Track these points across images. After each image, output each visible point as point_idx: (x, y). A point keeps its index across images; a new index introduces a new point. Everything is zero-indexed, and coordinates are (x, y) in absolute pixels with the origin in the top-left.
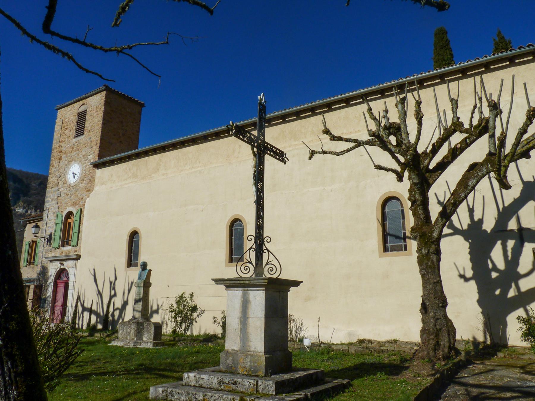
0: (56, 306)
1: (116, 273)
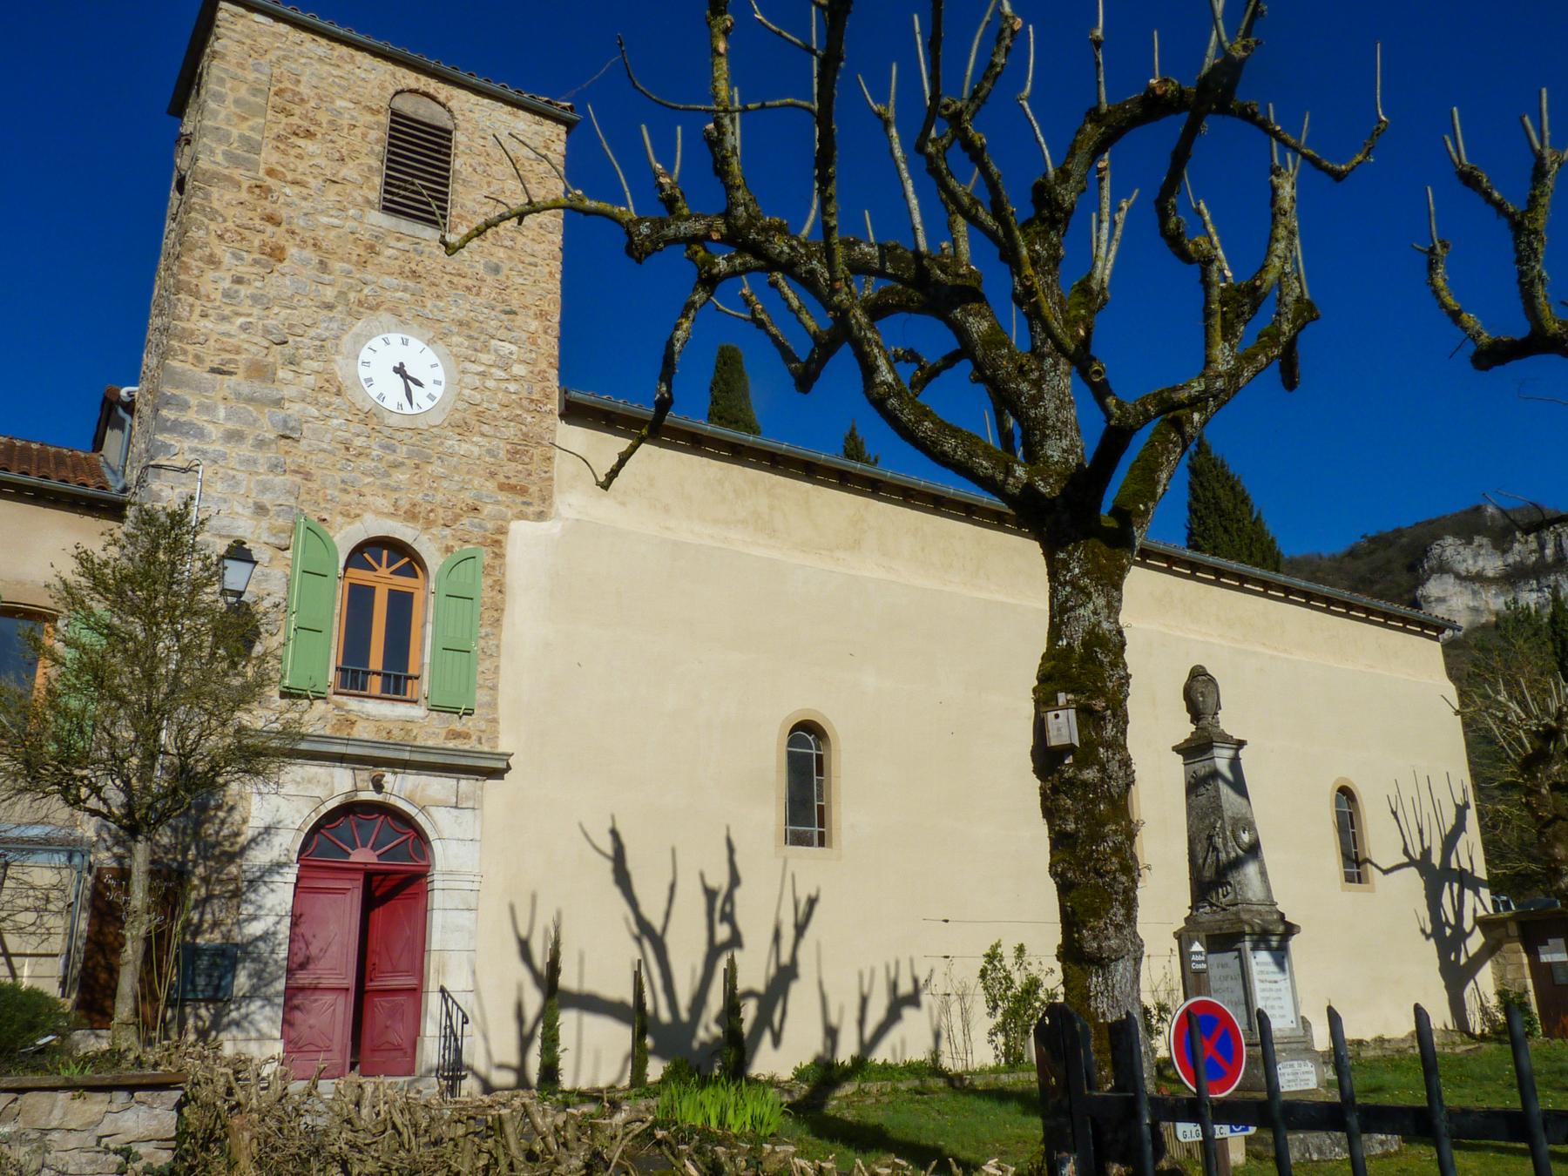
0: (302, 989)
1: (738, 858)
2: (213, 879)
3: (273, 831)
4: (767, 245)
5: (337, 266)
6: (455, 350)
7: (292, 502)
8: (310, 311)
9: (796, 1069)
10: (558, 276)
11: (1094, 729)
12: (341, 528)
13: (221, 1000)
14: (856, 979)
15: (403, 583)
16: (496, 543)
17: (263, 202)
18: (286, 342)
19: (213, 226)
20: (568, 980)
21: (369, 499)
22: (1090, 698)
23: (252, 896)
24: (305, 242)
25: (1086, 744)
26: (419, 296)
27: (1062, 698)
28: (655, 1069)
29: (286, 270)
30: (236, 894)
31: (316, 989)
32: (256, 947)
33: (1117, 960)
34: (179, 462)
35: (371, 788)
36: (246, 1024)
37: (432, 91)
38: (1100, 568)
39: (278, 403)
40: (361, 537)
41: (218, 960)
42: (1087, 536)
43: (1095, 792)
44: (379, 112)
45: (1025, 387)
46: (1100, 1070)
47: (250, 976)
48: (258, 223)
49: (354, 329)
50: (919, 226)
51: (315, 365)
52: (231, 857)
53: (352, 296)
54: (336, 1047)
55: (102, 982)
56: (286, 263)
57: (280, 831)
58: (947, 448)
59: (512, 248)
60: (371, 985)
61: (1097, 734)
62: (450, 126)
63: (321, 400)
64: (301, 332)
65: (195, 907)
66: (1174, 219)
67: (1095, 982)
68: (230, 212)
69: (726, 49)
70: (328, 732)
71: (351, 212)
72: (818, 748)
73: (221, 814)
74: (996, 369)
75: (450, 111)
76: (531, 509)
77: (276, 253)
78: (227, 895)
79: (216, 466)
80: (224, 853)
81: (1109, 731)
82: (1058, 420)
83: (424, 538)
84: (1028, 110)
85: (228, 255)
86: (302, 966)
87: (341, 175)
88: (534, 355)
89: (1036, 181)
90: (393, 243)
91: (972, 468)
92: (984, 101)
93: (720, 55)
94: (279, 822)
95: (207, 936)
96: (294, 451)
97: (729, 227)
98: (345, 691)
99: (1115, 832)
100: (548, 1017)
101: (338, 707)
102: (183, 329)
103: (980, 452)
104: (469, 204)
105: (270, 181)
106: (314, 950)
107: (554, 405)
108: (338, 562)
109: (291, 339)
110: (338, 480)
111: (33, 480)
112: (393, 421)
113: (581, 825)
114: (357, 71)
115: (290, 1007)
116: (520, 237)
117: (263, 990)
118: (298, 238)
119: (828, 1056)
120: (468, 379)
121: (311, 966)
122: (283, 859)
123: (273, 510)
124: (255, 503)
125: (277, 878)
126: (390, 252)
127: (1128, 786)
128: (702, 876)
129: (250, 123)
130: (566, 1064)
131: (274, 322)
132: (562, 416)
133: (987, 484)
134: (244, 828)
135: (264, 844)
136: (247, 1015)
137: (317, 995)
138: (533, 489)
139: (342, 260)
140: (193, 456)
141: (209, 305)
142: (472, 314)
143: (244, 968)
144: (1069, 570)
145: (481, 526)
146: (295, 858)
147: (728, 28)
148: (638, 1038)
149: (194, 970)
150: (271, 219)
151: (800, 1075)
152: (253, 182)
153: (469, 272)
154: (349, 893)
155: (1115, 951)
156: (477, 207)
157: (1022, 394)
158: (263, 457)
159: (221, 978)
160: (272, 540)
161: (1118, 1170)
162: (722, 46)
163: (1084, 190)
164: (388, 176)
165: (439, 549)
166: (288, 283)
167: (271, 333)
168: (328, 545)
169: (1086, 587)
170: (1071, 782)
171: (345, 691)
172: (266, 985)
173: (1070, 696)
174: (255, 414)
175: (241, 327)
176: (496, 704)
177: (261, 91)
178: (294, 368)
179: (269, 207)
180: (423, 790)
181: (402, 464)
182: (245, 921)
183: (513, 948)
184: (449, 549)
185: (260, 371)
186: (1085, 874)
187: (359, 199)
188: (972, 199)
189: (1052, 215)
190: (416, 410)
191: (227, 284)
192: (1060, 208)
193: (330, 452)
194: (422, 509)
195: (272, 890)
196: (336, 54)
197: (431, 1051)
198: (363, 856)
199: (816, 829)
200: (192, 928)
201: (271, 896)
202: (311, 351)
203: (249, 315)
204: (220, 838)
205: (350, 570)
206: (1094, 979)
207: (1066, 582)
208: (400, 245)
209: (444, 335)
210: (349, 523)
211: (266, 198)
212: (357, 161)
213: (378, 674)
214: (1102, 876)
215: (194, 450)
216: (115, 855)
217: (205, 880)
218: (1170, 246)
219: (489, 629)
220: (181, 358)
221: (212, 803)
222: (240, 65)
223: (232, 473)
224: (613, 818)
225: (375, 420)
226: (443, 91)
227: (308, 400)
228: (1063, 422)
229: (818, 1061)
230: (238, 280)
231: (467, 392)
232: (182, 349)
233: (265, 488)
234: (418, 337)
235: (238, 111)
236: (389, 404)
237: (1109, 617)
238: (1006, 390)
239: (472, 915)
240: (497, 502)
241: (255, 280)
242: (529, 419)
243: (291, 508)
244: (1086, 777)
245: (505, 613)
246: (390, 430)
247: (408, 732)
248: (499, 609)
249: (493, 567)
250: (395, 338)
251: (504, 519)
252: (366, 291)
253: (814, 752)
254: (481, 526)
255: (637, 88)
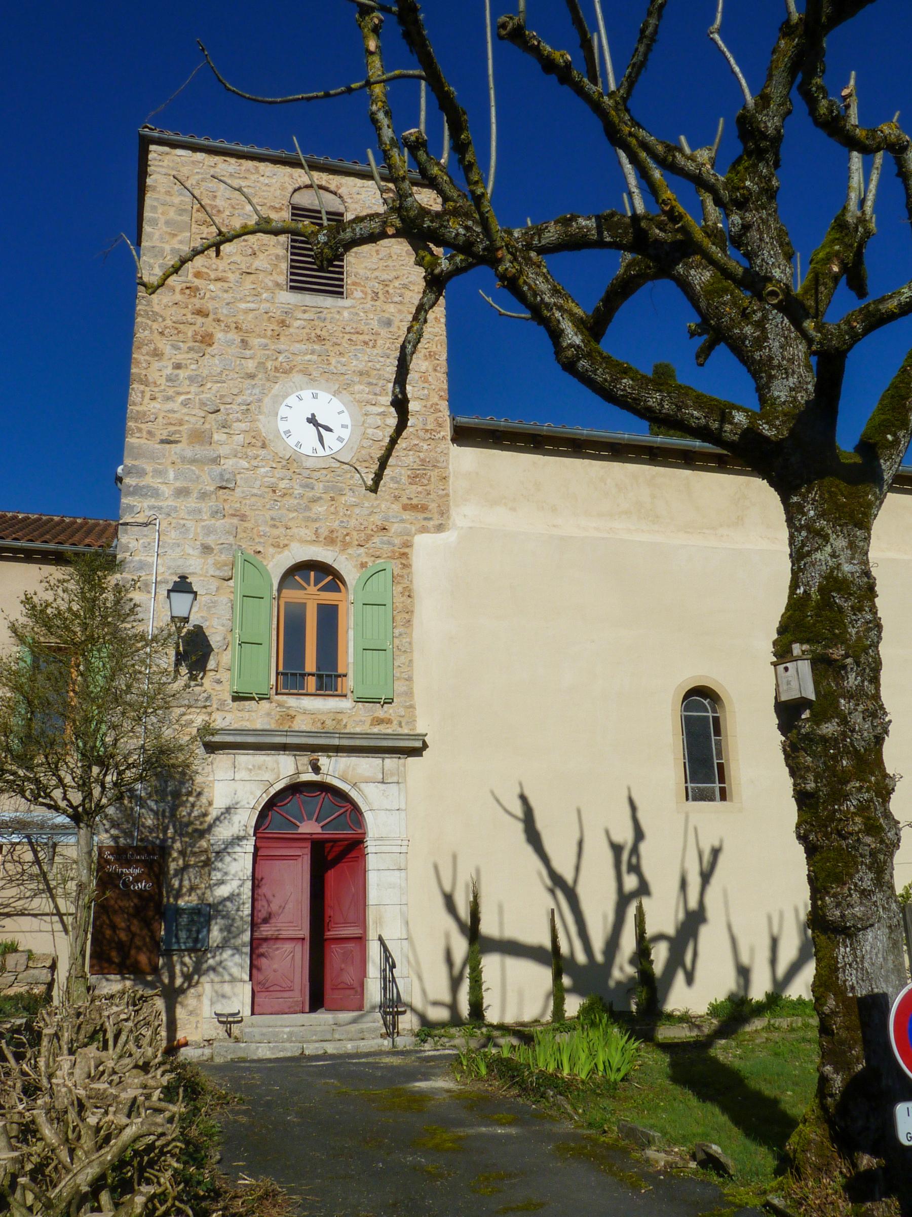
0: (266, 939)
1: (640, 815)
2: (188, 852)
3: (232, 811)
4: (443, 230)
5: (255, 342)
6: (357, 396)
7: (231, 539)
8: (236, 382)
9: (711, 1004)
10: (443, 320)
11: (835, 680)
12: (273, 557)
13: (200, 950)
14: (764, 922)
15: (329, 597)
16: (403, 556)
17: (193, 300)
18: (219, 411)
19: (155, 326)
20: (488, 927)
21: (295, 530)
22: (826, 647)
23: (219, 865)
24: (228, 327)
25: (825, 696)
26: (325, 357)
27: (797, 649)
28: (573, 1006)
29: (216, 352)
30: (207, 863)
31: (277, 939)
32: (225, 906)
33: (865, 928)
34: (141, 519)
35: (310, 770)
36: (221, 970)
37: (324, 183)
38: (839, 507)
39: (216, 460)
40: (291, 562)
41: (196, 918)
42: (821, 475)
43: (836, 747)
44: (281, 209)
45: (748, 330)
46: (851, 1049)
47: (221, 930)
48: (190, 317)
49: (274, 391)
50: (634, 190)
51: (243, 426)
52: (202, 834)
53: (269, 364)
54: (297, 987)
55: (108, 936)
56: (215, 346)
57: (239, 811)
58: (651, 403)
59: (401, 303)
60: (329, 934)
61: (837, 684)
62: (341, 209)
63: (250, 454)
64: (229, 400)
65: (175, 875)
66: (824, 103)
67: (843, 952)
68: (167, 313)
69: (377, 47)
70: (273, 726)
71: (264, 296)
72: (714, 711)
73: (192, 799)
74: (719, 317)
75: (340, 197)
76: (432, 523)
77: (207, 340)
78: (200, 864)
79: (170, 519)
80: (196, 830)
81: (852, 681)
82: (783, 358)
83: (342, 558)
84: (720, 43)
85: (168, 347)
86: (266, 921)
87: (254, 267)
88: (426, 392)
89: (738, 114)
90: (300, 315)
91: (682, 420)
92: (653, 40)
93: (372, 53)
94: (237, 803)
95: (187, 898)
96: (231, 498)
97: (403, 220)
98: (287, 691)
99: (859, 789)
100: (473, 962)
101: (280, 705)
102: (137, 411)
103: (690, 403)
104: (361, 272)
105: (197, 282)
106: (274, 907)
107: (447, 432)
108: (271, 585)
109: (222, 407)
110: (268, 517)
111: (51, 546)
112: (309, 463)
113: (492, 793)
114: (261, 179)
115: (255, 955)
116: (407, 292)
117: (232, 941)
118: (223, 325)
119: (742, 993)
120: (370, 420)
121: (273, 921)
122: (242, 834)
123: (217, 548)
124: (202, 545)
125: (238, 849)
126: (298, 323)
127: (879, 740)
128: (607, 833)
129: (179, 238)
130: (489, 999)
131: (208, 396)
132: (454, 440)
133: (702, 433)
134: (210, 809)
135: (226, 822)
136: (221, 962)
137: (279, 945)
138: (433, 506)
139: (259, 336)
140: (152, 513)
141: (156, 389)
142: (370, 364)
143: (216, 923)
144: (804, 514)
145: (389, 543)
146: (251, 832)
147: (376, 26)
148: (557, 976)
149: (177, 926)
150: (200, 312)
151: (714, 1010)
152: (184, 285)
153: (365, 328)
154: (300, 859)
155: (861, 919)
156: (369, 273)
157: (746, 337)
158: (206, 507)
159: (198, 932)
160: (217, 573)
161: (869, 1160)
162: (372, 45)
163: (789, 112)
164: (292, 260)
165: (355, 566)
166: (217, 362)
167: (206, 405)
168: (263, 572)
169: (822, 529)
170: (809, 738)
171: (287, 691)
172: (234, 937)
173: (805, 647)
174: (197, 472)
175: (182, 403)
176: (412, 693)
177: (185, 210)
178: (226, 431)
179: (197, 303)
180: (354, 769)
181: (320, 498)
182: (215, 885)
183: (440, 902)
184: (363, 565)
185: (200, 437)
186: (827, 836)
187: (270, 284)
188: (667, 146)
189: (757, 146)
190: (328, 452)
191: (169, 371)
192: (764, 136)
193: (260, 496)
194: (339, 534)
195: (235, 859)
196: (243, 168)
197: (374, 992)
198: (310, 827)
199: (717, 785)
200: (174, 892)
201: (234, 864)
202: (239, 415)
203: (188, 393)
204: (192, 819)
205: (284, 591)
206: (842, 950)
207: (802, 527)
208: (306, 316)
209: (348, 386)
210: (279, 553)
211: (195, 296)
212: (266, 253)
213: (313, 675)
214: (845, 838)
215: (152, 508)
216: (112, 836)
217: (182, 853)
218: (830, 135)
219: (402, 630)
220: (138, 435)
221: (184, 791)
222: (168, 193)
223: (182, 522)
224: (521, 785)
225: (295, 465)
226: (332, 181)
227: (240, 455)
228: (789, 360)
229: (731, 998)
230: (178, 366)
231: (370, 431)
232: (138, 428)
233: (209, 531)
234: (327, 390)
235: (169, 230)
236: (306, 450)
237: (853, 558)
238: (731, 337)
239: (403, 873)
240: (402, 521)
241: (191, 364)
242: (425, 447)
243: (231, 545)
244: (825, 731)
245: (415, 614)
246: (308, 472)
247: (339, 722)
248: (410, 612)
249: (402, 576)
250: (306, 394)
251: (409, 534)
252: (281, 359)
253: (710, 714)
254: (389, 543)
255: (229, 90)
